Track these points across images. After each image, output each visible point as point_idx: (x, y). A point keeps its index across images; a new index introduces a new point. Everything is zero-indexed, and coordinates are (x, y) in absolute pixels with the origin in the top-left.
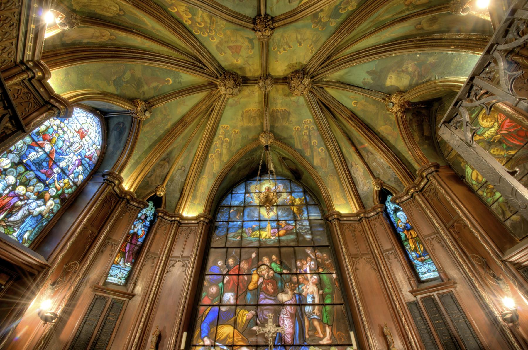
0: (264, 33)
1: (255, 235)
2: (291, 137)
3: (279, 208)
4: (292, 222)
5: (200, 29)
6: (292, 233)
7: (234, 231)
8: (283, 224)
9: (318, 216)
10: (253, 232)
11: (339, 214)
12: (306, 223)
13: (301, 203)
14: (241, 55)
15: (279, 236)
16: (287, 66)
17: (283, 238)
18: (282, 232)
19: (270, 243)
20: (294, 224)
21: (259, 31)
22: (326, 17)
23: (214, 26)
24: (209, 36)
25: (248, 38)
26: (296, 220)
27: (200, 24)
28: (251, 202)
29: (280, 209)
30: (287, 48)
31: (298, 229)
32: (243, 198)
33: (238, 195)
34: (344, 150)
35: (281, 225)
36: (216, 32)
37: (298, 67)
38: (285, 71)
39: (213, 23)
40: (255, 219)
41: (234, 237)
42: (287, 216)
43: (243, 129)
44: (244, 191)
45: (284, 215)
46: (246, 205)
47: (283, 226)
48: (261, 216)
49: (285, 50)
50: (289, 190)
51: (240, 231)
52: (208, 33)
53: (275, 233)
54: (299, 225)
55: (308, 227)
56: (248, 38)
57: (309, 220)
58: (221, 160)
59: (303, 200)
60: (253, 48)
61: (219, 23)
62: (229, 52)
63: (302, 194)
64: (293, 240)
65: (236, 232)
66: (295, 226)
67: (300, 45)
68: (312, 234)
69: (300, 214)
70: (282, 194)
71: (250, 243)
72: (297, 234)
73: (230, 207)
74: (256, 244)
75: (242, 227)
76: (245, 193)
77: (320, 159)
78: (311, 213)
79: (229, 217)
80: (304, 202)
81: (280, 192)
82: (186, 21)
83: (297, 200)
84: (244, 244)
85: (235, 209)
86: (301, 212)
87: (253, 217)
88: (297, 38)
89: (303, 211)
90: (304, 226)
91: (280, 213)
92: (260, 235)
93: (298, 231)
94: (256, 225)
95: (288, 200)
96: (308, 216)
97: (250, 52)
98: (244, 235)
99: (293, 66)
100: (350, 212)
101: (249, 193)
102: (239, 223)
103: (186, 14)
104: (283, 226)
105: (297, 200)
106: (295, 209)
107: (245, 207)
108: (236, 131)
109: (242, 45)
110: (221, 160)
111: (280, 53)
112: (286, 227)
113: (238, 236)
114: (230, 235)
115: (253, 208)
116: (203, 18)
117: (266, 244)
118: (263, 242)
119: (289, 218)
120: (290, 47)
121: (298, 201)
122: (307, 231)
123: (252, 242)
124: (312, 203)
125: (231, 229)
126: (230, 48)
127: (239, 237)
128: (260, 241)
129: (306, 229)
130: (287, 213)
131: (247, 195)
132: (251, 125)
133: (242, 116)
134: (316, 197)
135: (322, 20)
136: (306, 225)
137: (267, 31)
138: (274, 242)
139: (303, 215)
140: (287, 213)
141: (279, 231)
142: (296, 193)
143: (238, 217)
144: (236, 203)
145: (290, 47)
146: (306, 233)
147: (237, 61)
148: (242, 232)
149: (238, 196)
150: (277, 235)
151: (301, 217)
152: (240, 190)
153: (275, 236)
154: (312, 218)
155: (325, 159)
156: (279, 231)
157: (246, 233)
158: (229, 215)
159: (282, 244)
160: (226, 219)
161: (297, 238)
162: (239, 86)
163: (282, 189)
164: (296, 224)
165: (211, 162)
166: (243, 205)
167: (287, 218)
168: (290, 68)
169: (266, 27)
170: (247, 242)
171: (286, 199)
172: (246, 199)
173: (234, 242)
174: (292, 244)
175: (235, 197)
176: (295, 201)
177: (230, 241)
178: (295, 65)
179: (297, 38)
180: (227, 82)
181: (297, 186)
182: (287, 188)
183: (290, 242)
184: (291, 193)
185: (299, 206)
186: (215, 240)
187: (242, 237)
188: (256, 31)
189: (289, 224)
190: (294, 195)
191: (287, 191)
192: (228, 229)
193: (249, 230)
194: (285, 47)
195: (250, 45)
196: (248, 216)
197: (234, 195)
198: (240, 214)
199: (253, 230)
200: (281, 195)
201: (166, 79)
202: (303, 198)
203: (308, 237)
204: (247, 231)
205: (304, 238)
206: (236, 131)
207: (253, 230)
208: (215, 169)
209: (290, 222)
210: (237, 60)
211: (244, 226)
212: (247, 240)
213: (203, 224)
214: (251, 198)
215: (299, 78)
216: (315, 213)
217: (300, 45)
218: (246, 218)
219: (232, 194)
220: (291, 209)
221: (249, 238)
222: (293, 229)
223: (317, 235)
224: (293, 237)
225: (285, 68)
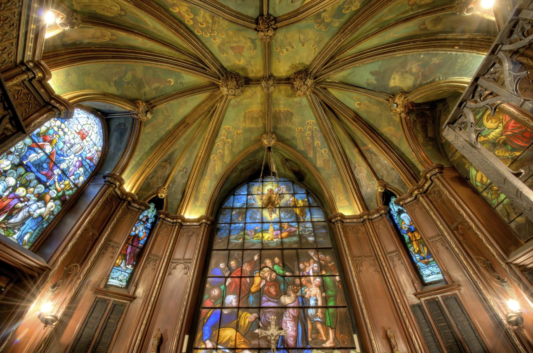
0: (267, 34)
1: (257, 237)
2: (294, 138)
3: (282, 209)
4: (295, 224)
5: (202, 29)
6: (294, 235)
7: (236, 233)
8: (285, 226)
9: (321, 217)
10: (255, 234)
11: (342, 216)
12: (309, 225)
13: (304, 204)
14: (243, 56)
15: (282, 238)
16: (289, 67)
17: (285, 240)
18: (284, 234)
19: (273, 245)
20: (297, 226)
21: (262, 31)
22: (330, 17)
23: (216, 26)
24: (211, 36)
25: (250, 38)
26: (298, 222)
27: (202, 24)
28: (253, 204)
29: (282, 211)
30: (290, 49)
31: (301, 231)
32: (246, 200)
33: (240, 196)
34: (347, 152)
35: (284, 227)
36: (218, 33)
37: (301, 68)
38: (288, 71)
39: (215, 24)
40: (257, 221)
41: (236, 239)
42: (290, 218)
43: (246, 130)
44: (246, 193)
45: (287, 217)
46: (248, 207)
47: (286, 228)
48: (264, 217)
49: (287, 50)
50: (292, 192)
51: (242, 233)
52: (210, 33)
53: (277, 235)
54: (302, 227)
55: (311, 229)
56: (250, 38)
57: (312, 222)
58: (223, 162)
59: (306, 202)
60: (255, 48)
61: (221, 23)
62: (231, 52)
63: (305, 196)
64: (296, 243)
65: (238, 234)
66: (298, 228)
67: (303, 45)
68: (315, 236)
69: (302, 216)
70: (285, 195)
71: (252, 245)
72: (300, 236)
73: (233, 208)
74: (259, 246)
75: (244, 229)
76: (248, 195)
77: (323, 161)
78: (314, 215)
79: (231, 219)
80: (307, 204)
81: (282, 194)
82: (188, 21)
83: (300, 201)
84: (246, 246)
85: (238, 210)
86: (304, 214)
87: (256, 219)
88: (300, 39)
89: (306, 213)
90: (307, 228)
91: (282, 215)
92: (263, 237)
93: (300, 233)
94: (258, 227)
95: (291, 202)
96: (311, 218)
97: (253, 52)
98: (246, 237)
99: (296, 66)
100: (354, 214)
101: (252, 195)
102: (241, 225)
103: (188, 14)
104: (286, 228)
105: (300, 201)
106: (298, 211)
107: (247, 208)
108: (239, 132)
109: (244, 45)
110: (223, 162)
111: (283, 53)
112: (288, 229)
113: (240, 239)
114: (232, 237)
115: (255, 210)
116: (205, 19)
117: (269, 246)
118: (266, 244)
119: (292, 220)
120: (293, 48)
121: (300, 203)
122: (310, 233)
123: (254, 244)
124: (315, 204)
125: (233, 231)
126: (232, 48)
127: (242, 239)
128: (262, 243)
129: (308, 231)
130: (289, 215)
131: (249, 197)
132: (253, 126)
133: (245, 117)
134: (319, 199)
135: (325, 20)
136: (309, 227)
137: (270, 31)
138: (277, 244)
139: (306, 217)
140: (289, 215)
141: (281, 233)
142: (299, 195)
143: (240, 219)
144: (238, 205)
145: (293, 48)
146: (309, 235)
147: (240, 61)
148: (244, 234)
149: (241, 198)
150: (280, 237)
151: (304, 219)
152: (242, 191)
153: (278, 238)
154: (315, 220)
155: (329, 160)
156: (281, 233)
157: (248, 235)
158: (231, 217)
159: (285, 246)
160: (229, 221)
161: (300, 240)
162: (242, 86)
163: (284, 190)
164: (299, 226)
165: (213, 164)
166: (245, 206)
167: (289, 220)
168: (293, 68)
169: (269, 27)
170: (249, 244)
171: (289, 200)
172: (248, 201)
173: (236, 244)
174: (295, 246)
175: (237, 199)
176: (298, 203)
177: (232, 243)
178: (297, 65)
179: (300, 39)
180: (229, 83)
181: (300, 188)
182: (290, 190)
183: (293, 244)
184: (294, 194)
185: (302, 208)
186: (217, 242)
187: (244, 239)
188: (258, 31)
189: (292, 226)
190: (297, 196)
191: (290, 192)
192: (230, 231)
193: (251, 232)
194: (288, 47)
195: (252, 46)
196: (250, 218)
197: (236, 197)
198: (242, 216)
199: (256, 231)
200: (284, 197)
201: (168, 80)
202: (306, 200)
203: (311, 239)
204: (249, 233)
205: (307, 240)
206: (239, 132)
207: (256, 231)
208: (217, 170)
209: (293, 224)
210: (240, 61)
211: (247, 227)
212: (249, 242)
213: (205, 226)
214: (254, 200)
215: (301, 79)
216: (318, 215)
217: (303, 45)
218: (248, 220)
219: (234, 195)
220: (294, 211)
221: (251, 240)
222: (296, 231)
223: (320, 237)
224: (295, 239)
225: (288, 68)
